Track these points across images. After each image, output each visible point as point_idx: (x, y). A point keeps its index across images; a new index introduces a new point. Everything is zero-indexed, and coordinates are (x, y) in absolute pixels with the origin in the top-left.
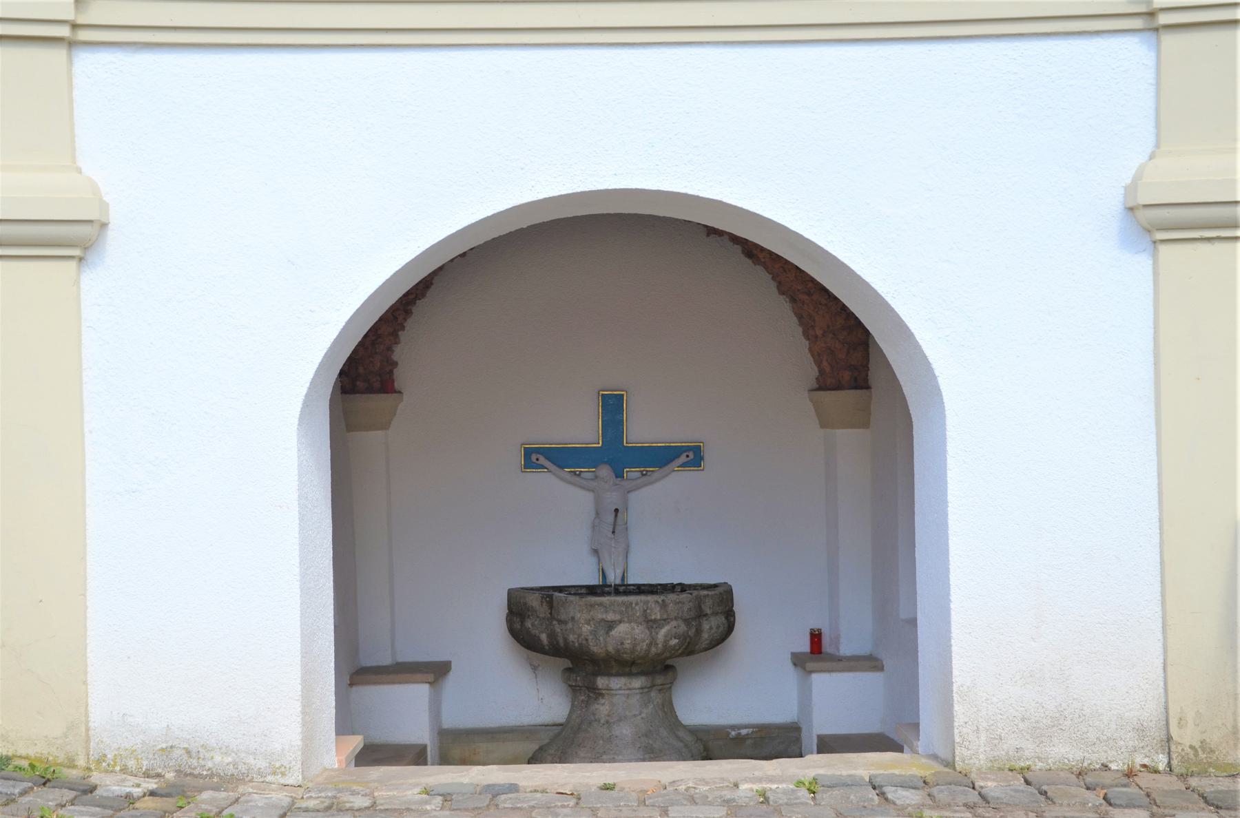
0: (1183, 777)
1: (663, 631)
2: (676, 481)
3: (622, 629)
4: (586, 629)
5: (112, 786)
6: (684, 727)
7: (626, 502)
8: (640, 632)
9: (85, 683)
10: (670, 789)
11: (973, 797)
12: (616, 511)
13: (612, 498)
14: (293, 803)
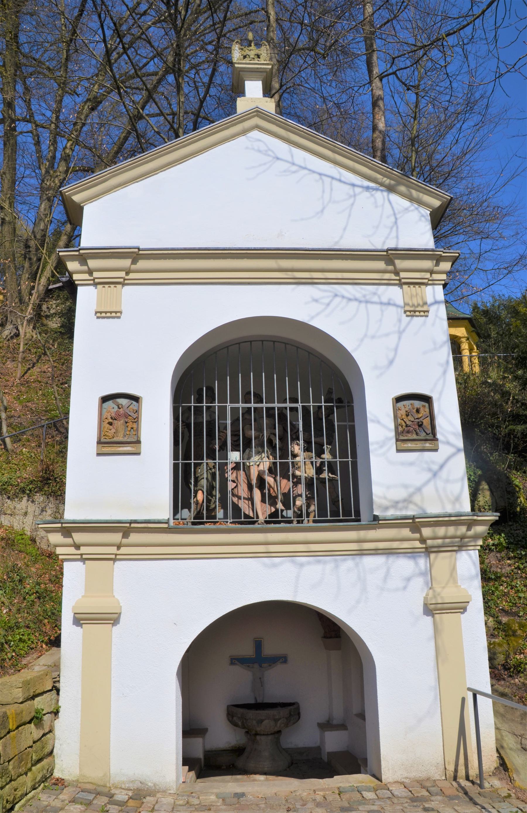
1: (279, 722)
2: (279, 668)
3: (266, 722)
5: (121, 796)
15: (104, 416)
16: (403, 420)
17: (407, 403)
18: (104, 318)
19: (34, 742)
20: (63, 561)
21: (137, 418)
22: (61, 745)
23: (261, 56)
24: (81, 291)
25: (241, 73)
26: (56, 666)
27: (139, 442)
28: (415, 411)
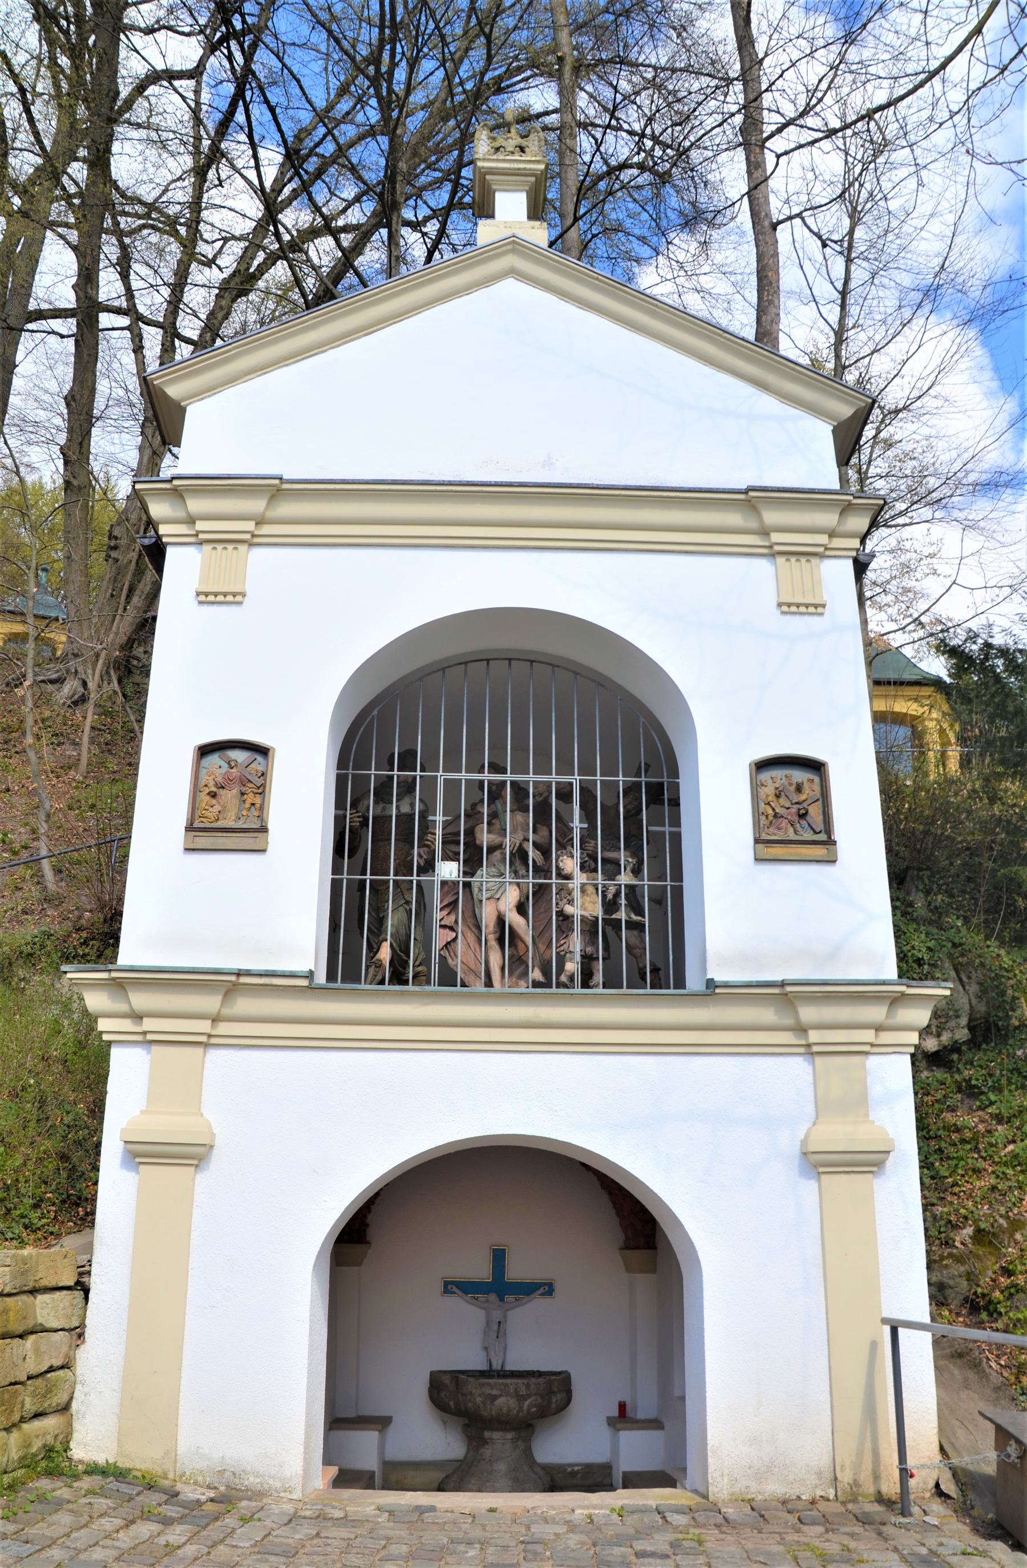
0: (844, 1503)
1: (527, 1403)
2: (536, 1306)
3: (502, 1400)
4: (479, 1400)
6: (539, 1464)
7: (505, 1316)
8: (512, 1403)
9: (177, 1425)
10: (531, 1512)
11: (720, 1519)
12: (500, 1322)
13: (497, 1315)
14: (296, 1513)
15: (202, 781)
16: (769, 804)
17: (779, 774)
18: (213, 603)
19: (29, 1378)
20: (109, 1043)
21: (263, 785)
22: (86, 1395)
23: (527, 150)
24: (172, 555)
25: (488, 177)
26: (89, 1248)
27: (264, 830)
28: (793, 788)
